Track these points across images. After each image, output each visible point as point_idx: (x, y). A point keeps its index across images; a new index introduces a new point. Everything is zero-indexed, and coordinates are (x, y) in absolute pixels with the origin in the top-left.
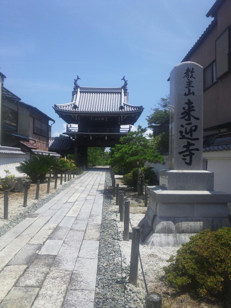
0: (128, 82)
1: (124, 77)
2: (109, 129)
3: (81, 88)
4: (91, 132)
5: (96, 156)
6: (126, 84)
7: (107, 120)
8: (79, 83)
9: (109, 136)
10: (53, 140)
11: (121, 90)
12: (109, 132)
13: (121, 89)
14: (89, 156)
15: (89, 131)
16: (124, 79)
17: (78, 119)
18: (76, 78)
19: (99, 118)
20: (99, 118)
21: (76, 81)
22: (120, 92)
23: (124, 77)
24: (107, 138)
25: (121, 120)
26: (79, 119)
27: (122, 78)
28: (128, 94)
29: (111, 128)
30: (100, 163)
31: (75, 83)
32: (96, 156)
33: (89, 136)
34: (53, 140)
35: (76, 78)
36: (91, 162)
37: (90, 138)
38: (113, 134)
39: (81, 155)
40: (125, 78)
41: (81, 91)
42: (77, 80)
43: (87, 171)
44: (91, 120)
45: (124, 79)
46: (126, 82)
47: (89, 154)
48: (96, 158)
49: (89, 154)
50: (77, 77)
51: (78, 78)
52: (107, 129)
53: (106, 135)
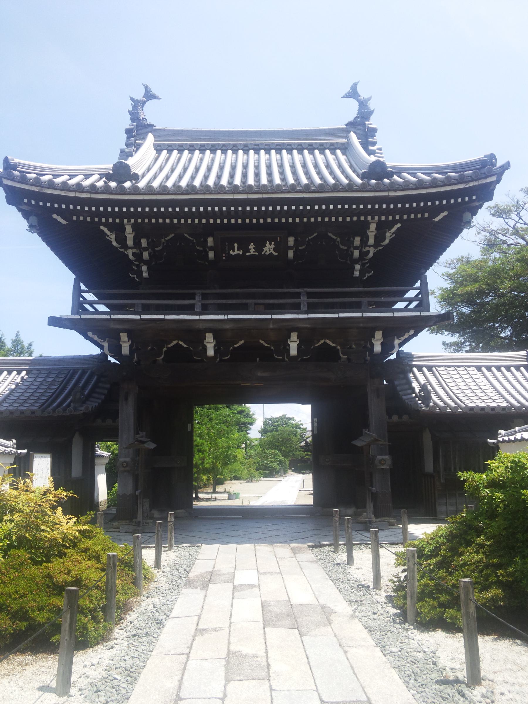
0: (372, 105)
1: (354, 88)
2: (310, 295)
3: (159, 134)
4: (205, 310)
5: (229, 448)
6: (365, 113)
7: (291, 254)
8: (151, 113)
9: (309, 334)
10: (19, 372)
11: (347, 138)
12: (312, 308)
13: (343, 132)
14: (203, 452)
15: (198, 308)
16: (353, 93)
17: (138, 256)
18: (139, 95)
19: (252, 246)
20: (252, 246)
21: (137, 105)
22: (343, 144)
23: (354, 88)
24: (299, 347)
25: (363, 255)
26: (146, 255)
27: (348, 89)
28: (381, 154)
29: (151, 546)
30: (236, 471)
31: (134, 115)
32: (229, 448)
33: (194, 334)
34: (19, 372)
35: (139, 95)
36: (206, 471)
37: (205, 349)
38: (335, 315)
39: (152, 446)
40: (359, 90)
41: (159, 145)
42: (144, 103)
43: (193, 543)
44: (211, 255)
45: (353, 93)
46: (363, 104)
47: (202, 444)
48: (227, 456)
49: (202, 444)
50: (143, 91)
51: (149, 95)
52: (297, 295)
53: (294, 330)
